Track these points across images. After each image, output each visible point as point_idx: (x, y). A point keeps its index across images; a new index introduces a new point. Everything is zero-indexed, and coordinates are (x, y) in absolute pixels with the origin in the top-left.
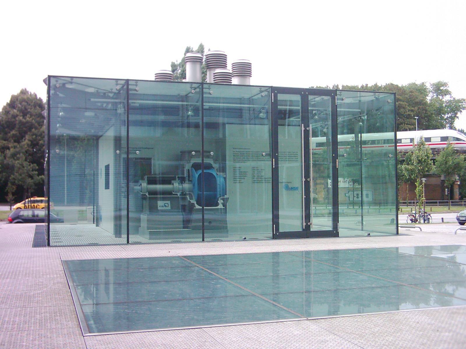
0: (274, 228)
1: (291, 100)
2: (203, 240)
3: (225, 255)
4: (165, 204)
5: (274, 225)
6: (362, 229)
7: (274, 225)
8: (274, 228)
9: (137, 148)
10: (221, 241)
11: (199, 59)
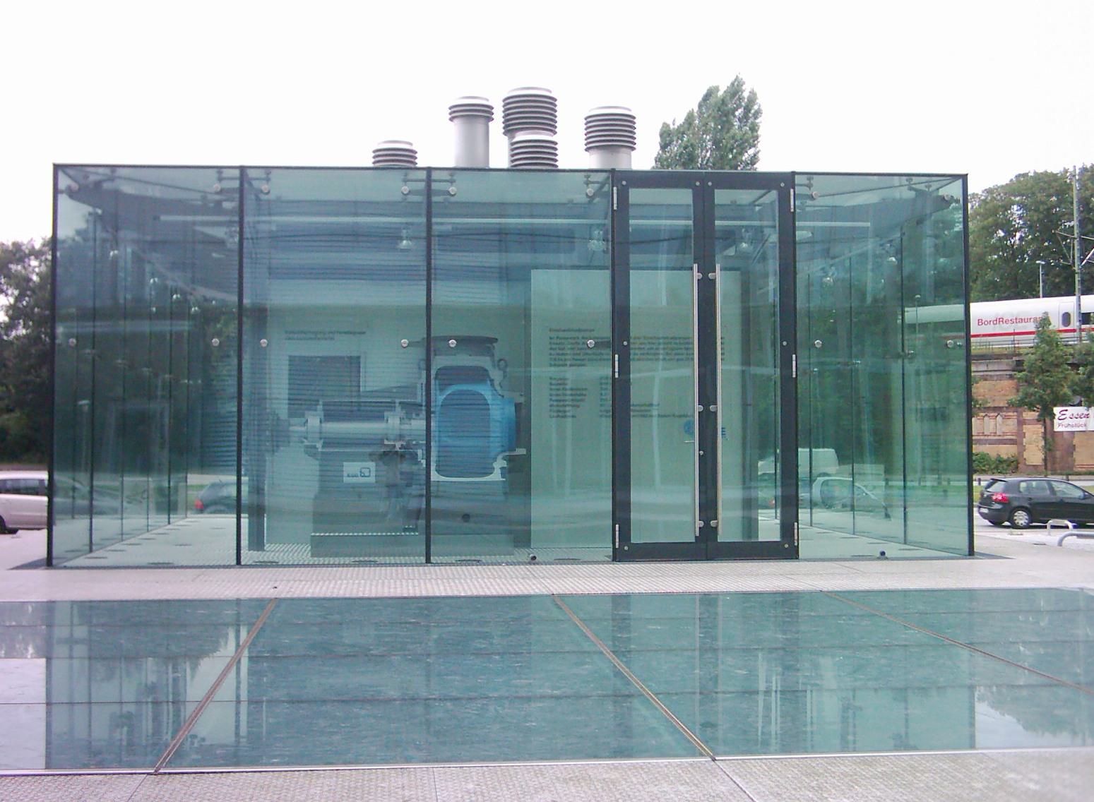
0: (617, 533)
1: (834, 204)
2: (428, 561)
3: (526, 598)
4: (363, 470)
5: (617, 526)
6: (905, 540)
7: (617, 526)
8: (617, 533)
9: (324, 333)
10: (478, 562)
11: (483, 111)
